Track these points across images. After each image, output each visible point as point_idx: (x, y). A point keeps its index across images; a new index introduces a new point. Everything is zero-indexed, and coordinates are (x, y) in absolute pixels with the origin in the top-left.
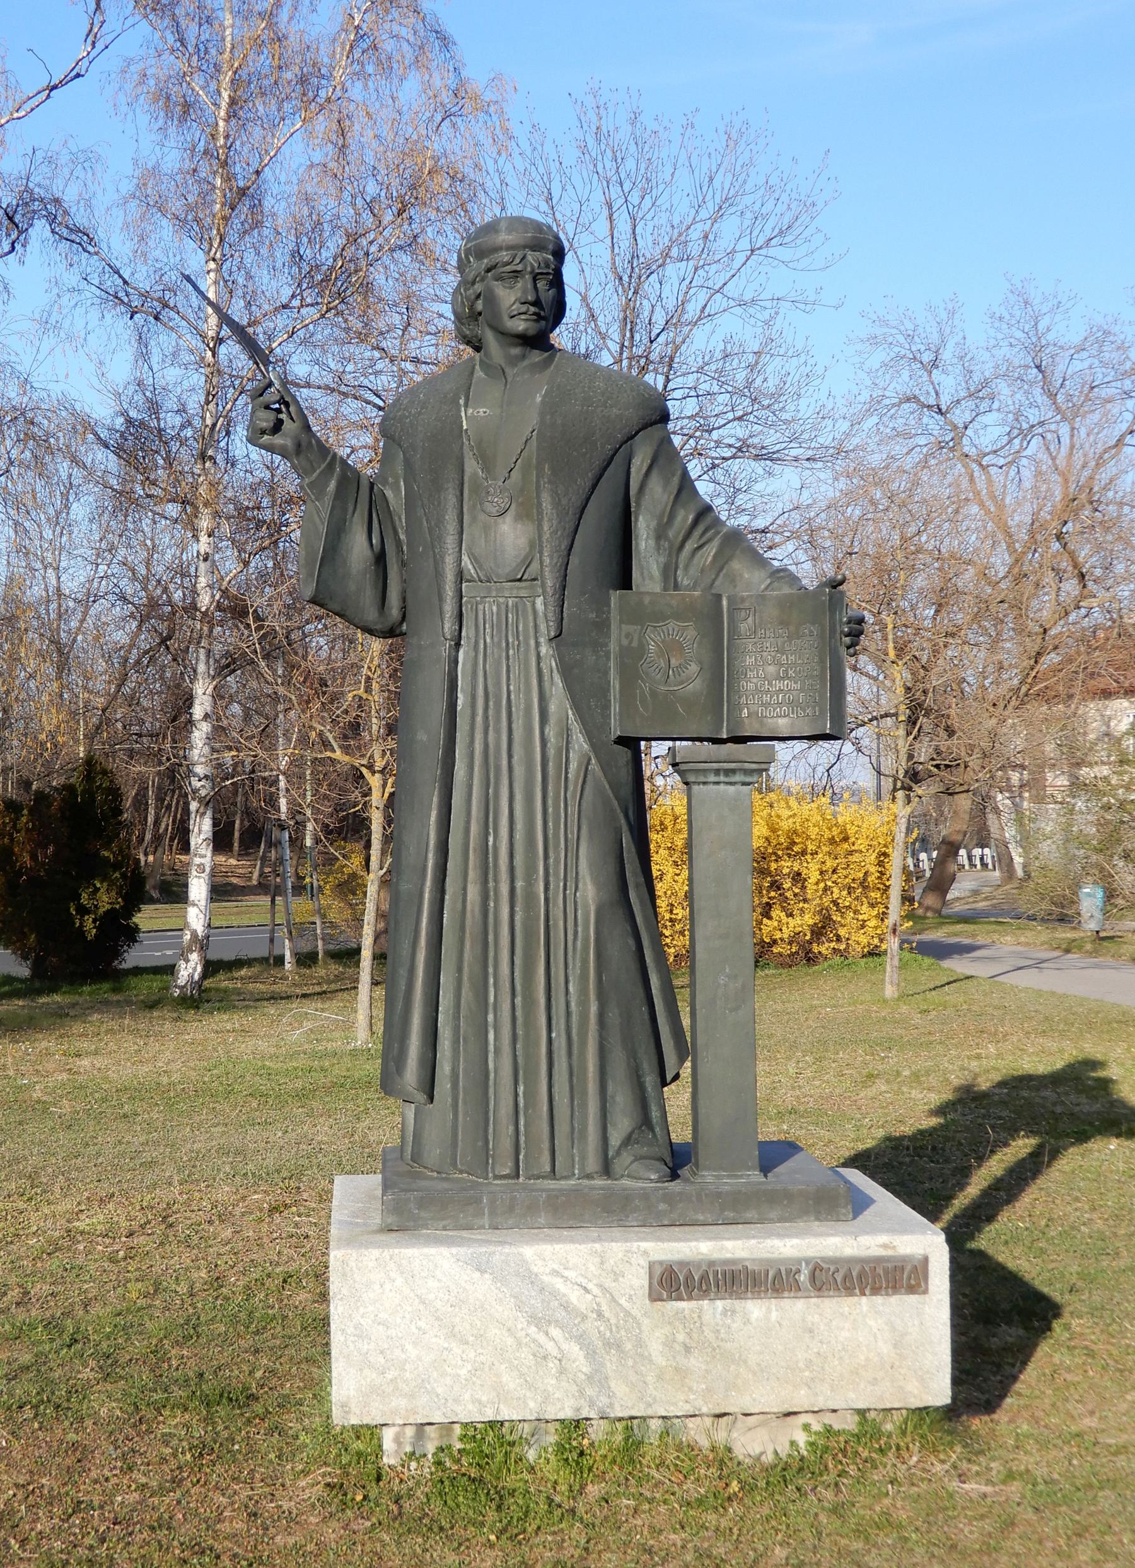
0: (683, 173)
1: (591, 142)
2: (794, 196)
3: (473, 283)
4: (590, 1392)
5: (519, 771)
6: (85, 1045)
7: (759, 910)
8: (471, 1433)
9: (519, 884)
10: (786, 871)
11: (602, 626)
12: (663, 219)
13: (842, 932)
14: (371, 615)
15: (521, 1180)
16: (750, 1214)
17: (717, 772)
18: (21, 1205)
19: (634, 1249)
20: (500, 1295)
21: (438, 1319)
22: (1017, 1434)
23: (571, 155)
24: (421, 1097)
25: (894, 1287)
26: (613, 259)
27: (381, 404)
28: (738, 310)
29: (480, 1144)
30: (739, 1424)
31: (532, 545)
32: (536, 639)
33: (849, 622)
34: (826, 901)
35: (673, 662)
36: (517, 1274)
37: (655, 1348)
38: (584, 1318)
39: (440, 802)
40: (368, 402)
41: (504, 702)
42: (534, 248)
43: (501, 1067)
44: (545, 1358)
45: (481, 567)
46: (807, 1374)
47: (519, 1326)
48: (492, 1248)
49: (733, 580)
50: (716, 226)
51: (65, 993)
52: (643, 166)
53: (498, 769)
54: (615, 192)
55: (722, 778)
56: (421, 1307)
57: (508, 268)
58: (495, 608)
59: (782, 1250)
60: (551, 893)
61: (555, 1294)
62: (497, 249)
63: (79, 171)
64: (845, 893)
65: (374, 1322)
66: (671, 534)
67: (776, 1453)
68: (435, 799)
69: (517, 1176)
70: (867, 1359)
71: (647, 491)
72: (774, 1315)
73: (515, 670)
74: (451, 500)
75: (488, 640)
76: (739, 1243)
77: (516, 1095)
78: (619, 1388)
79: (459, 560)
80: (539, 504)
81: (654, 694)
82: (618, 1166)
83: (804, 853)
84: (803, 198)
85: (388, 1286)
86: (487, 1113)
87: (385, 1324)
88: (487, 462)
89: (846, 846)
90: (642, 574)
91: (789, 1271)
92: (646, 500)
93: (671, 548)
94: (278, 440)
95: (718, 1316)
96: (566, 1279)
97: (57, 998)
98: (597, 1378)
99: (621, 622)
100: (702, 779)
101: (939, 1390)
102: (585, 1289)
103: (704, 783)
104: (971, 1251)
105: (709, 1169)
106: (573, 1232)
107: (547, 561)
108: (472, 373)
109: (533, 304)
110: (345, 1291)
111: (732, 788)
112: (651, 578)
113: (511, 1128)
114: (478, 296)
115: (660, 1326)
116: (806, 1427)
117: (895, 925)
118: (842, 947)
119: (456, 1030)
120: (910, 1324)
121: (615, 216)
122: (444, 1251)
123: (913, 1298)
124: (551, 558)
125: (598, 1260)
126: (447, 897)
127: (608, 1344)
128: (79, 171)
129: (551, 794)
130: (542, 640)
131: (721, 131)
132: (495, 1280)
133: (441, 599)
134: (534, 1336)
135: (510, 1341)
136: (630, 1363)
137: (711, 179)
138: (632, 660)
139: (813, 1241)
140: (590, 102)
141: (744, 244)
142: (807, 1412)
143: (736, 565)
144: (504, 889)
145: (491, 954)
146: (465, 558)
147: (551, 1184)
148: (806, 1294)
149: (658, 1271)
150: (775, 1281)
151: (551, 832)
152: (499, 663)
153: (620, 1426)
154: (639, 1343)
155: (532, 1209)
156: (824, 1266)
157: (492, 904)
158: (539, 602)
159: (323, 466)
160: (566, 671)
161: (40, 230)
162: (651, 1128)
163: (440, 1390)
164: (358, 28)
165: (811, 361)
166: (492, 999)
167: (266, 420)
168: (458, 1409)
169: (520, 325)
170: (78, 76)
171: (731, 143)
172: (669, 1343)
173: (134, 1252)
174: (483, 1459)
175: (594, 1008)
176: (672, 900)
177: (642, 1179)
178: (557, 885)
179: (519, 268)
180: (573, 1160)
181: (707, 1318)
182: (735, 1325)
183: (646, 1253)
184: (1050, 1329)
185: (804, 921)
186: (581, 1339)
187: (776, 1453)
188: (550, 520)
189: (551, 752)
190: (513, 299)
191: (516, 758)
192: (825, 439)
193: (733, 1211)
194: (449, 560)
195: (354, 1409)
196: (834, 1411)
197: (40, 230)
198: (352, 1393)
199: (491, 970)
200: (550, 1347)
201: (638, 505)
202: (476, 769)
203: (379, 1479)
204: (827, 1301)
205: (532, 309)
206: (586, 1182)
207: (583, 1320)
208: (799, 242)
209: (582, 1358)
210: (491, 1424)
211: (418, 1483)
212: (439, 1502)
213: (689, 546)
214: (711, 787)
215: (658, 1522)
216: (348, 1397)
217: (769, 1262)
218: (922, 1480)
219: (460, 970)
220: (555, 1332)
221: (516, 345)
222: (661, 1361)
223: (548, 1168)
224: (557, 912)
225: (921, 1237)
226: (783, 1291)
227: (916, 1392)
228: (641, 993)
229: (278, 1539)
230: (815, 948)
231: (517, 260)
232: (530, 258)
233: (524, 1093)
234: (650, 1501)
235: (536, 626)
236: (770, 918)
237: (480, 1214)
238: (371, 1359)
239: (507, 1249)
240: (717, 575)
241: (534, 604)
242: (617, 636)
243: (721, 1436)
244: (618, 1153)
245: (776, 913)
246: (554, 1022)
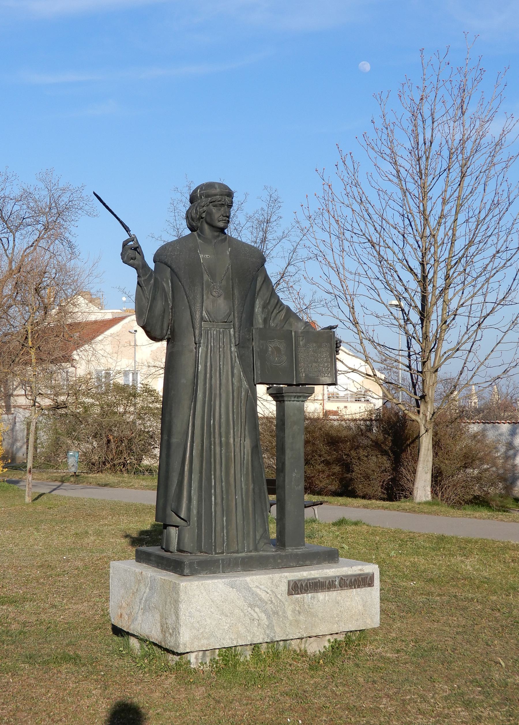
3: (203, 207)
4: (267, 632)
16: (308, 562)
17: (295, 397)
19: (283, 576)
37: (289, 613)
44: (253, 620)
47: (245, 608)
48: (236, 579)
53: (215, 394)
56: (212, 603)
57: (220, 203)
58: (215, 332)
61: (257, 595)
67: (319, 651)
70: (355, 612)
75: (212, 344)
76: (316, 571)
78: (277, 629)
79: (202, 313)
85: (200, 596)
87: (199, 611)
88: (212, 276)
91: (332, 581)
102: (267, 592)
105: (288, 547)
107: (236, 315)
110: (186, 599)
115: (290, 604)
116: (329, 641)
117: (30, 469)
125: (271, 581)
127: (274, 613)
132: (237, 591)
134: (250, 612)
135: (242, 614)
136: (281, 620)
143: (291, 320)
146: (204, 312)
154: (284, 612)
157: (213, 447)
160: (240, 357)
166: (213, 484)
168: (224, 642)
172: (294, 611)
174: (226, 662)
181: (306, 600)
183: (286, 577)
186: (265, 612)
188: (238, 300)
195: (188, 646)
198: (188, 639)
200: (255, 615)
201: (258, 295)
206: (249, 554)
209: (265, 619)
213: (276, 311)
217: (327, 578)
220: (257, 609)
221: (217, 232)
222: (291, 618)
224: (237, 450)
233: (226, 520)
238: (194, 625)
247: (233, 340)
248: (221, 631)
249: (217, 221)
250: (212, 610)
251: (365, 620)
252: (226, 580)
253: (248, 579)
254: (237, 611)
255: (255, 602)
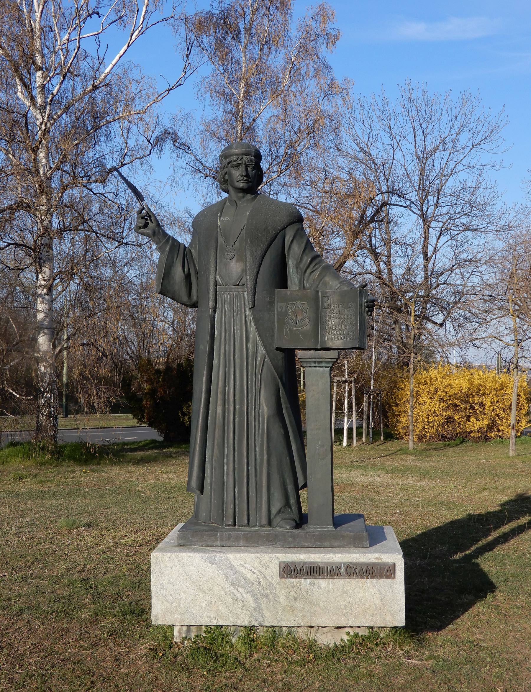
0: (445, 115)
1: (407, 104)
2: (491, 124)
3: (224, 168)
5: (238, 361)
6: (172, 469)
7: (465, 418)
8: (209, 630)
9: (237, 407)
10: (476, 402)
11: (272, 303)
12: (436, 133)
13: (500, 428)
14: (185, 299)
15: (236, 527)
16: (327, 544)
17: (315, 362)
18: (104, 532)
20: (219, 574)
21: (194, 582)
22: (444, 640)
23: (399, 109)
24: (198, 492)
26: (416, 151)
27: (314, 210)
28: (468, 170)
29: (220, 511)
30: (320, 631)
31: (243, 271)
32: (245, 308)
33: (367, 302)
34: (493, 414)
35: (299, 318)
36: (226, 566)
37: (282, 598)
38: (253, 584)
39: (207, 373)
40: (310, 210)
41: (232, 334)
42: (246, 155)
43: (229, 480)
44: (237, 600)
45: (223, 280)
46: (344, 611)
47: (227, 587)
49: (325, 284)
50: (458, 136)
51: (176, 447)
52: (428, 112)
53: (230, 360)
54: (416, 123)
55: (317, 365)
56: (187, 577)
58: (229, 296)
59: (334, 559)
60: (249, 410)
61: (241, 574)
62: (231, 155)
63: (185, 122)
64: (502, 411)
65: (168, 583)
66: (301, 266)
68: (205, 372)
69: (235, 526)
70: (370, 606)
71: (292, 249)
72: (331, 586)
73: (237, 320)
74: (213, 254)
77: (235, 492)
78: (267, 614)
80: (246, 256)
81: (291, 330)
82: (277, 521)
83: (484, 394)
84: (494, 124)
85: (174, 568)
86: (223, 499)
88: (226, 239)
89: (502, 392)
90: (291, 282)
92: (292, 252)
93: (301, 271)
94: (146, 231)
95: (308, 586)
97: (171, 450)
98: (258, 609)
99: (278, 302)
100: (309, 365)
101: (400, 620)
103: (310, 367)
104: (474, 563)
106: (252, 549)
108: (225, 204)
109: (245, 176)
110: (157, 570)
111: (321, 369)
112: (295, 284)
113: (232, 506)
114: (226, 174)
116: (348, 633)
118: (500, 434)
119: (212, 465)
120: (388, 591)
121: (416, 133)
122: (197, 555)
123: (389, 581)
124: (250, 276)
125: (258, 560)
126: (210, 411)
127: (262, 595)
128: (185, 122)
129: (250, 371)
130: (247, 309)
131: (460, 98)
132: (217, 567)
133: (208, 293)
135: (222, 593)
136: (272, 603)
137: (456, 118)
138: (283, 316)
139: (347, 555)
140: (406, 87)
141: (470, 144)
143: (327, 279)
144: (232, 409)
145: (226, 435)
146: (218, 276)
147: (247, 529)
148: (344, 577)
149: (283, 566)
150: (330, 571)
151: (250, 386)
152: (230, 318)
153: (270, 630)
154: (275, 595)
155: (237, 539)
156: (351, 566)
158: (246, 293)
159: (164, 241)
160: (256, 321)
161: (169, 144)
162: (290, 507)
163: (194, 612)
164: (293, 62)
165: (496, 191)
167: (142, 222)
168: (202, 620)
169: (241, 185)
170: (180, 85)
171: (464, 103)
172: (287, 596)
173: (137, 553)
175: (265, 457)
176: (429, 413)
177: (283, 528)
178: (252, 407)
179: (240, 162)
180: (257, 520)
181: (303, 586)
182: (314, 589)
184: (486, 597)
185: (485, 423)
186: (251, 593)
187: (335, 643)
189: (250, 353)
190: (238, 175)
191: (236, 356)
192: (502, 223)
193: (320, 543)
194: (212, 277)
195: (160, 618)
196: (359, 627)
197: (169, 144)
198: (159, 611)
199: (226, 441)
200: (239, 596)
201: (288, 254)
202: (221, 360)
203: (171, 647)
204: (353, 580)
205: (245, 178)
207: (252, 585)
208: (493, 142)
209: (252, 601)
210: (217, 627)
211: (185, 650)
212: (191, 658)
213: (309, 271)
214: (313, 368)
215: (276, 670)
216: (158, 613)
218: (391, 657)
219: (214, 441)
220: (241, 589)
221: (240, 192)
223: (246, 522)
224: (252, 418)
225: (392, 555)
226: (334, 576)
227: (390, 620)
228: (286, 452)
229: (122, 670)
230: (489, 434)
231: (239, 159)
232: (244, 158)
234: (276, 661)
235: (244, 303)
236: (469, 421)
237: (216, 540)
239: (222, 555)
240: (319, 283)
241: (244, 294)
242: (279, 306)
243: (313, 636)
244: (275, 516)
245: (472, 419)
246: (250, 463)
247: (247, 304)
248: (198, 608)
249: (236, 182)
250: (187, 584)
251: (384, 616)
252: (204, 555)
253: (230, 556)
254: (216, 589)
255: (237, 581)
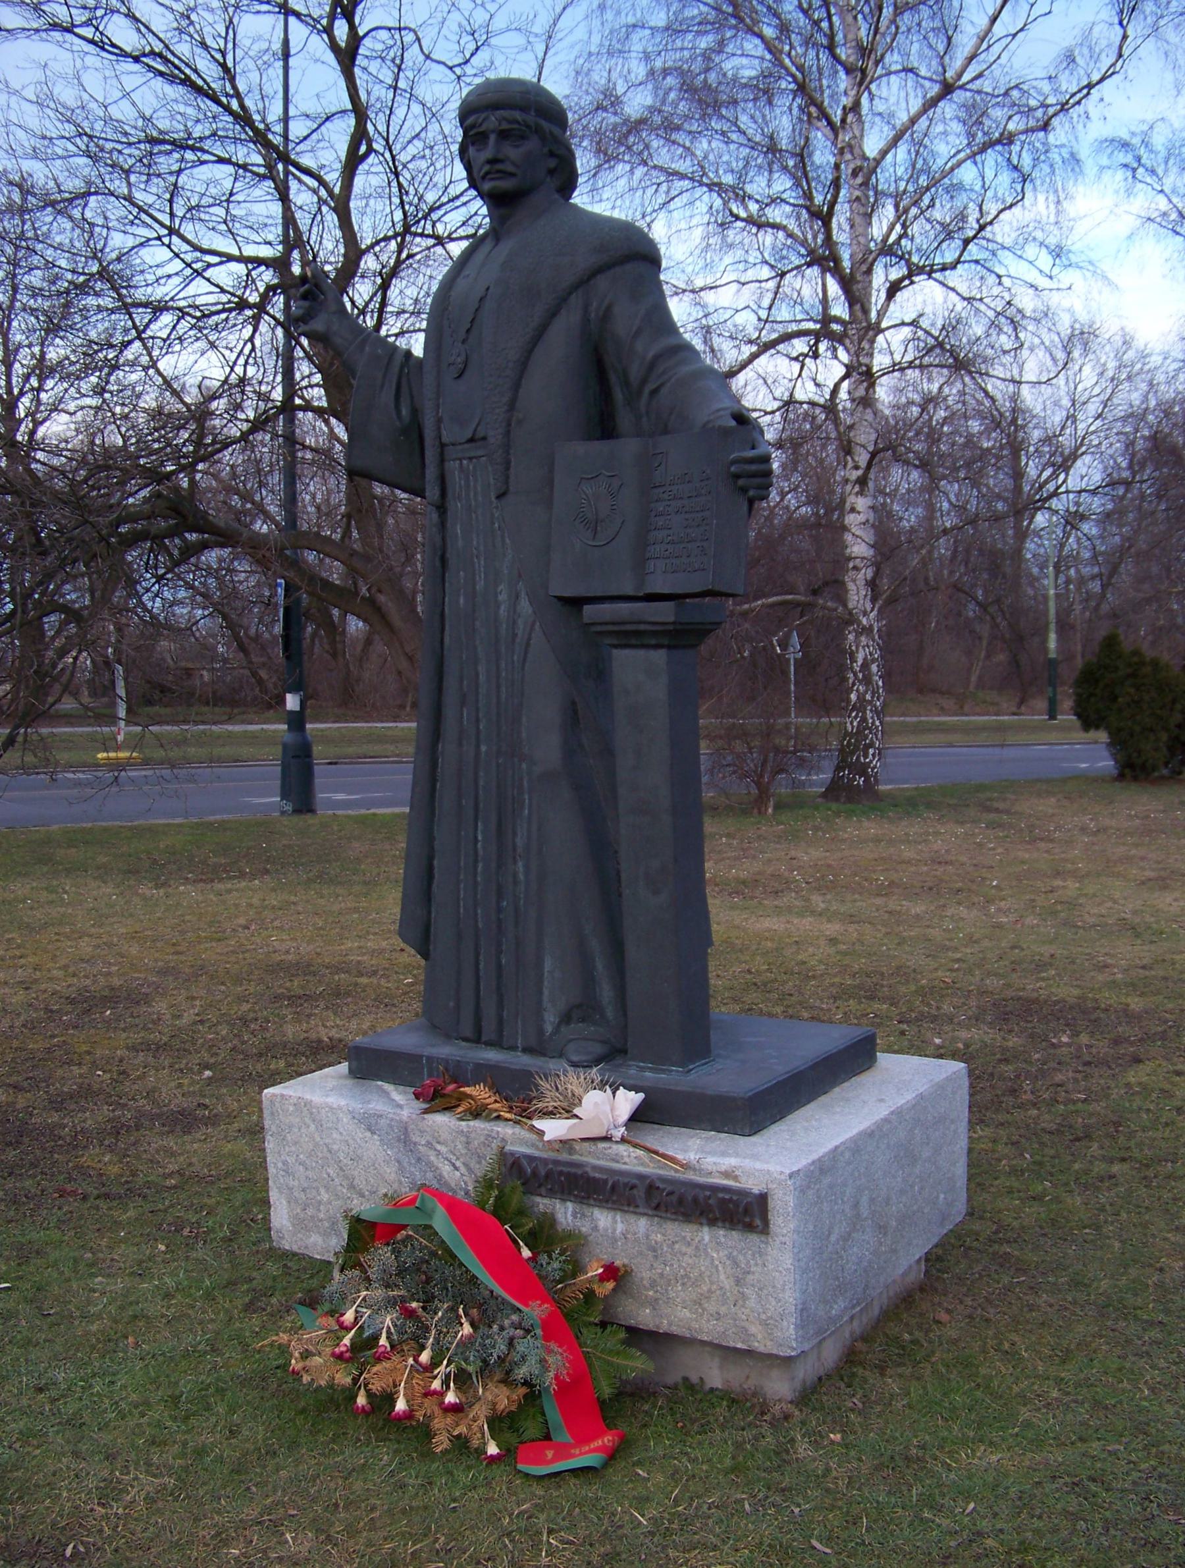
25: (732, 1221)
72: (620, 1227)
96: (439, 1153)
110: (274, 1128)
142: (517, 386)
156: (658, 1184)
